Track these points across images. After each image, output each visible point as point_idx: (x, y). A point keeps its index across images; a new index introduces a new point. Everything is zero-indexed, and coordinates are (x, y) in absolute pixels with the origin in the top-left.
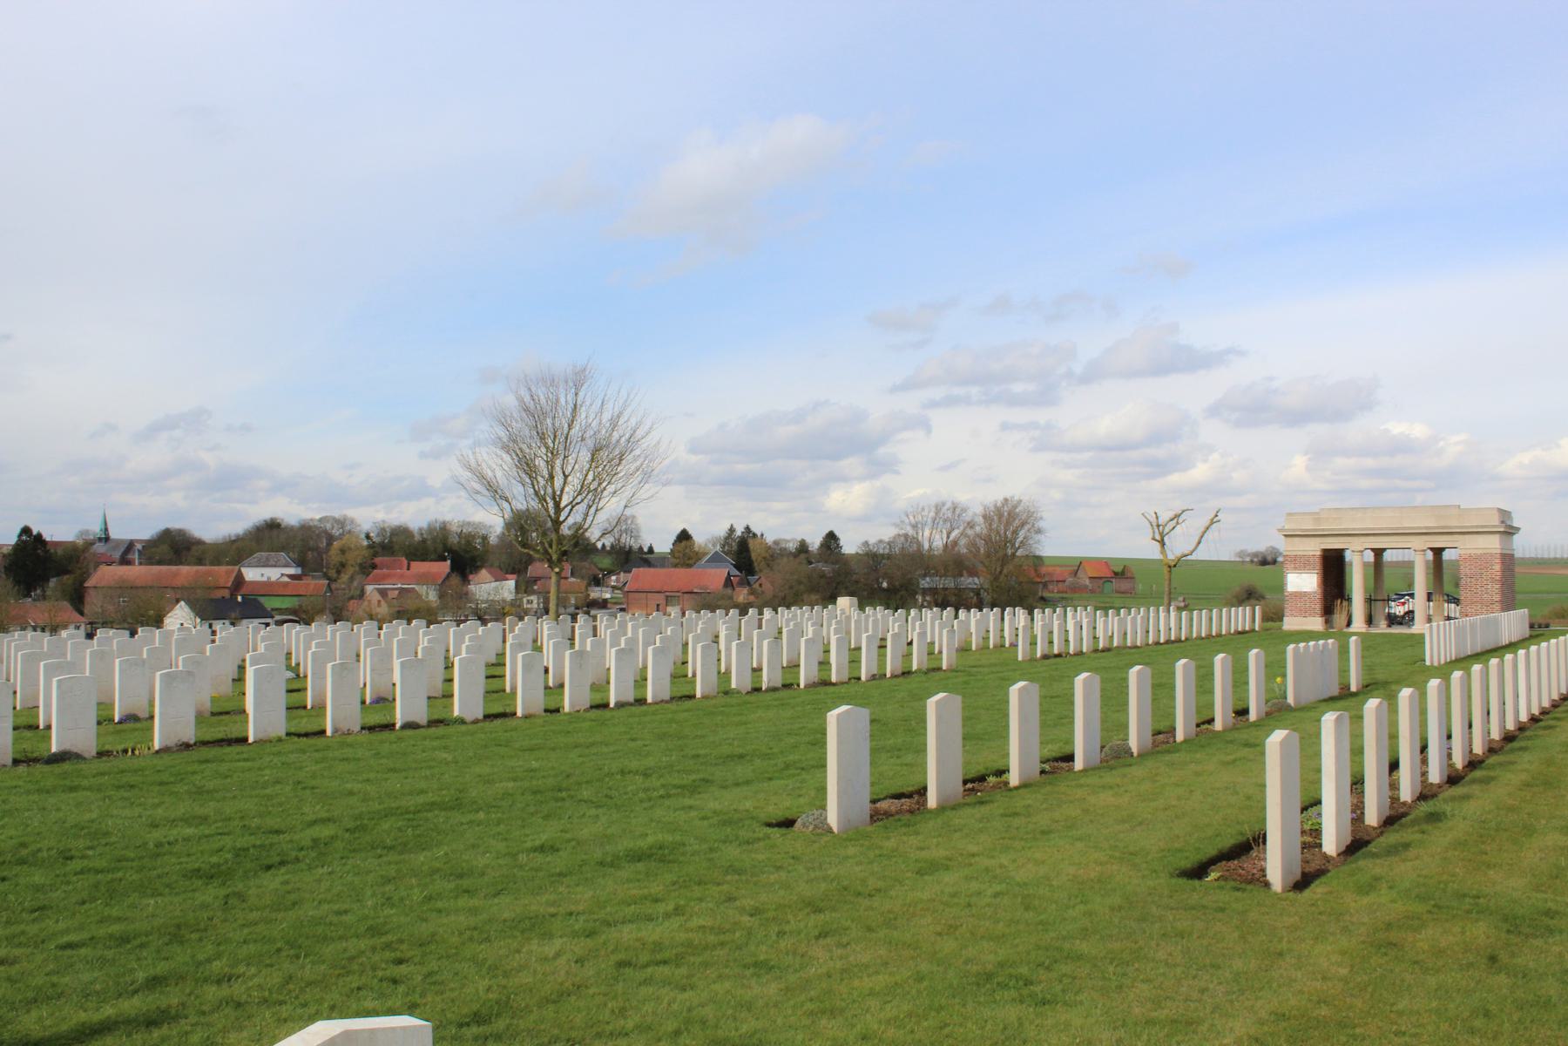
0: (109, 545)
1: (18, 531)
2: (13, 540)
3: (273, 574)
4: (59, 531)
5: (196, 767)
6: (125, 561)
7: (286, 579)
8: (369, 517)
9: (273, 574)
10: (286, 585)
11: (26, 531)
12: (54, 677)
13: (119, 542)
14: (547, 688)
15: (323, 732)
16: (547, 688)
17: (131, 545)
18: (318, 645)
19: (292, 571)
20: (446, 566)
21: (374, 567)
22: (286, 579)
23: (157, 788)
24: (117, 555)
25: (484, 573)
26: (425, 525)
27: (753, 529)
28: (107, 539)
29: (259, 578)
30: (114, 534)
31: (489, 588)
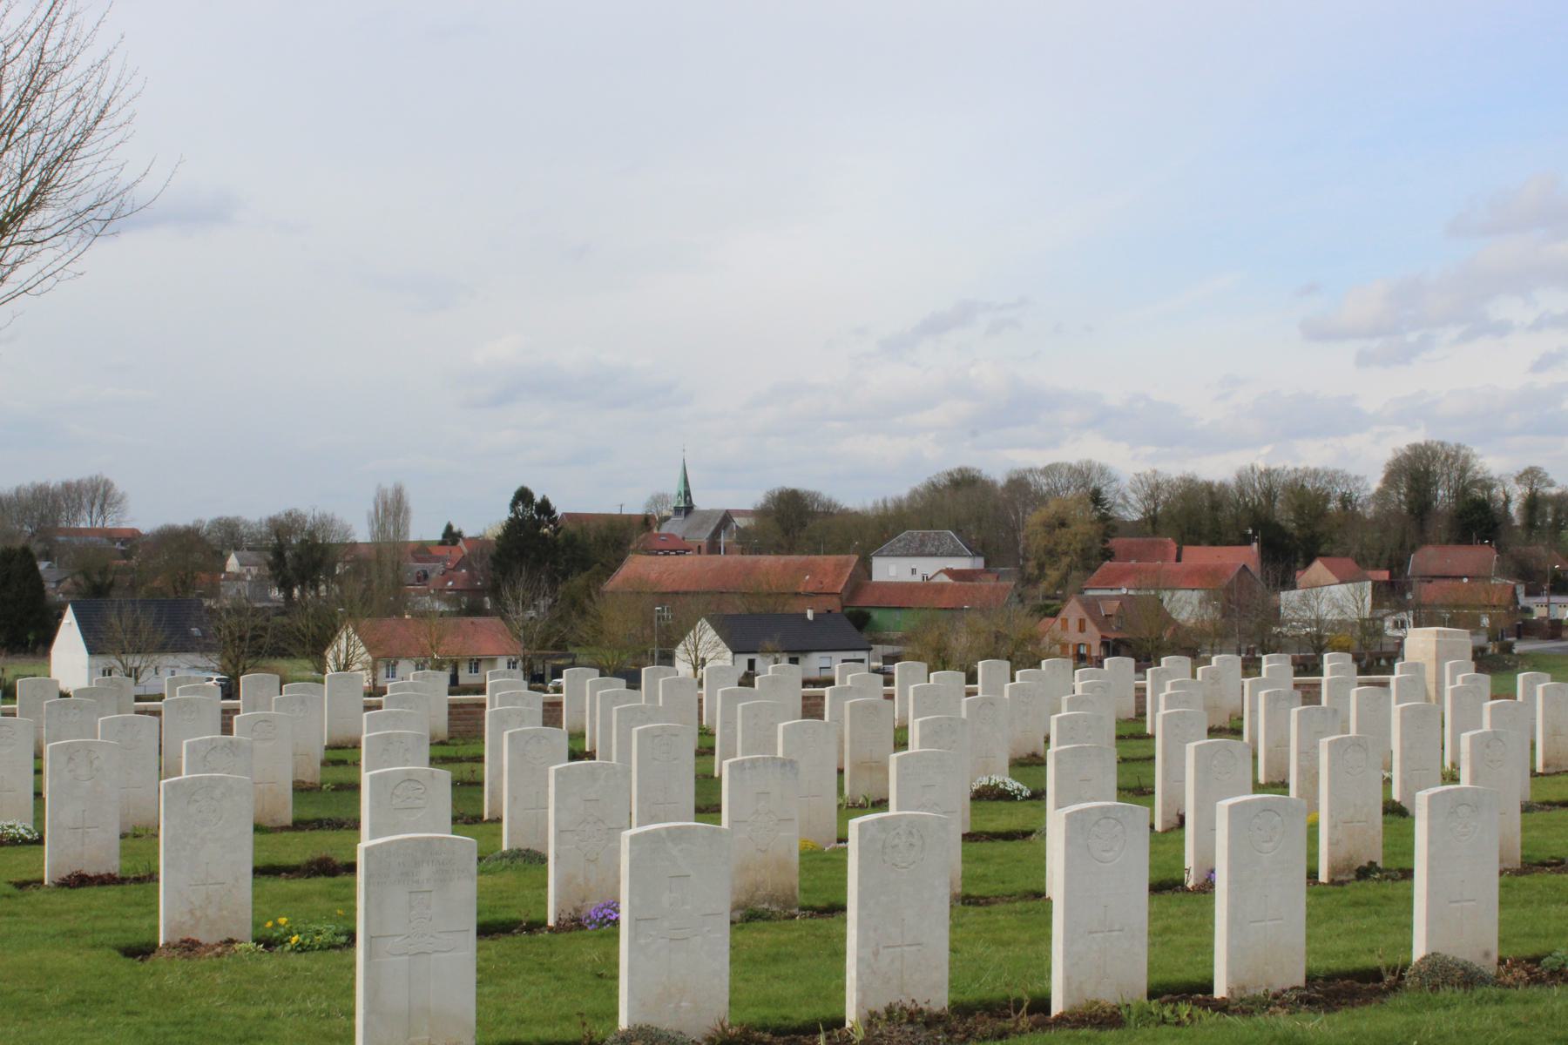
0: (692, 519)
1: (510, 497)
2: (505, 514)
3: (928, 568)
4: (575, 495)
5: (99, 924)
6: (713, 547)
7: (945, 579)
8: (1131, 467)
9: (928, 568)
10: (941, 588)
11: (523, 496)
12: (126, 760)
13: (707, 515)
14: (1534, 774)
15: (42, 882)
16: (1534, 774)
17: (727, 518)
18: (1174, 686)
19: (963, 564)
20: (1250, 554)
21: (1108, 555)
22: (945, 579)
23: (1351, 910)
24: (703, 537)
25: (1318, 566)
26: (1217, 482)
27: (455, 529)
28: (688, 509)
29: (907, 577)
30: (701, 502)
31: (1330, 596)
